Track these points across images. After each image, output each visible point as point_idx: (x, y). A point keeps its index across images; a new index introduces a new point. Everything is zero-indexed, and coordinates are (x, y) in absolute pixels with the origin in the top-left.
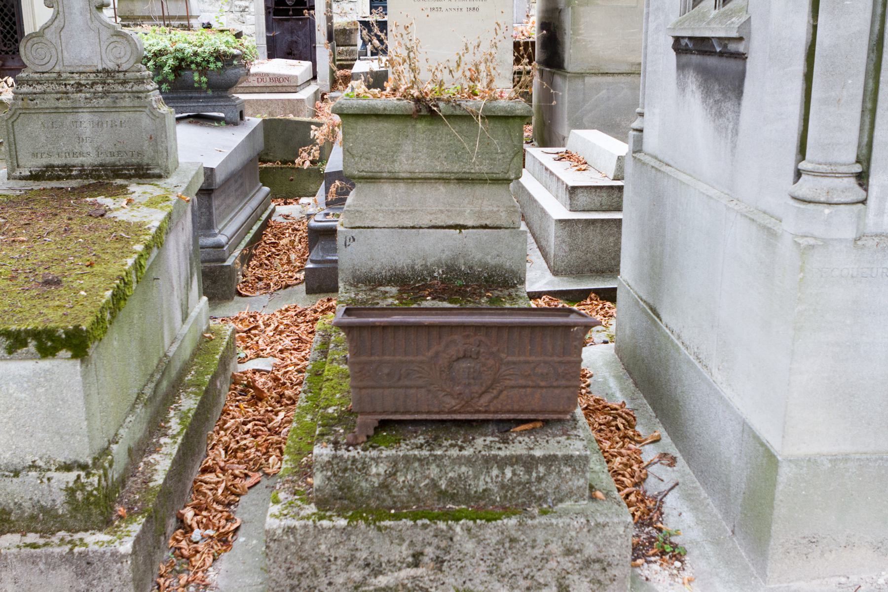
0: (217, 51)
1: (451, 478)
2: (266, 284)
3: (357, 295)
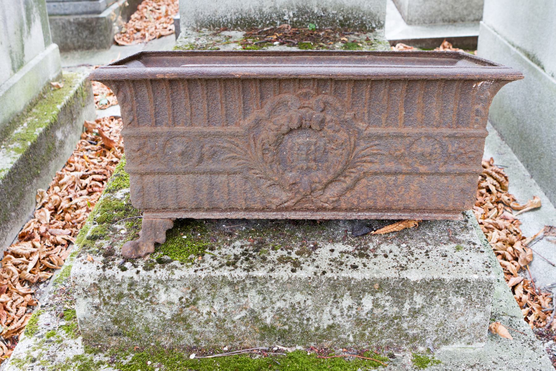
1: (280, 309)
2: (142, 35)
3: (197, 40)
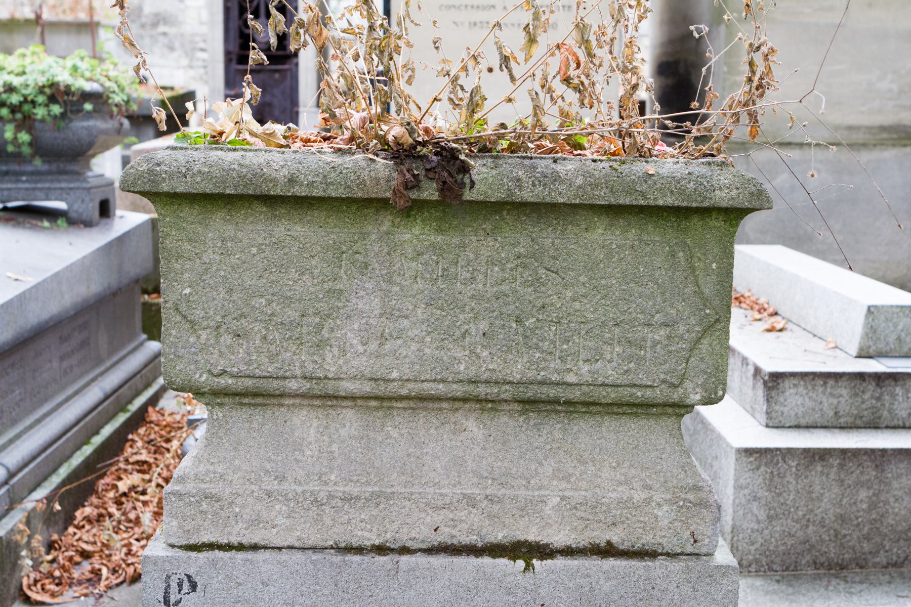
0: (53, 85)
